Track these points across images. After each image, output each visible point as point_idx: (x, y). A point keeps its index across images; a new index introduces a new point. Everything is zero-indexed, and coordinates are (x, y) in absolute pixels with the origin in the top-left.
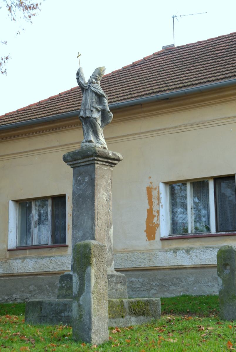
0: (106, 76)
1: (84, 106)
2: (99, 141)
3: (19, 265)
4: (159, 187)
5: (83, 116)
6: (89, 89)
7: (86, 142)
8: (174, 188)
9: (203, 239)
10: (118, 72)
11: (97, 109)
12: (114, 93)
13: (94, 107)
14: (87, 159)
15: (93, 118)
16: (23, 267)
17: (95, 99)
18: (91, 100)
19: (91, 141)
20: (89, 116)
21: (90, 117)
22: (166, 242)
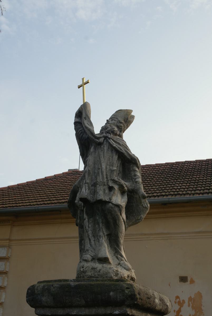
0: (21, 185)
1: (90, 177)
2: (122, 260)
5: (89, 198)
6: (105, 143)
7: (93, 259)
10: (32, 182)
11: (121, 187)
12: (32, 198)
13: (115, 182)
15: (113, 204)
17: (117, 166)
18: (108, 167)
19: (105, 260)
20: (104, 199)
21: (106, 203)
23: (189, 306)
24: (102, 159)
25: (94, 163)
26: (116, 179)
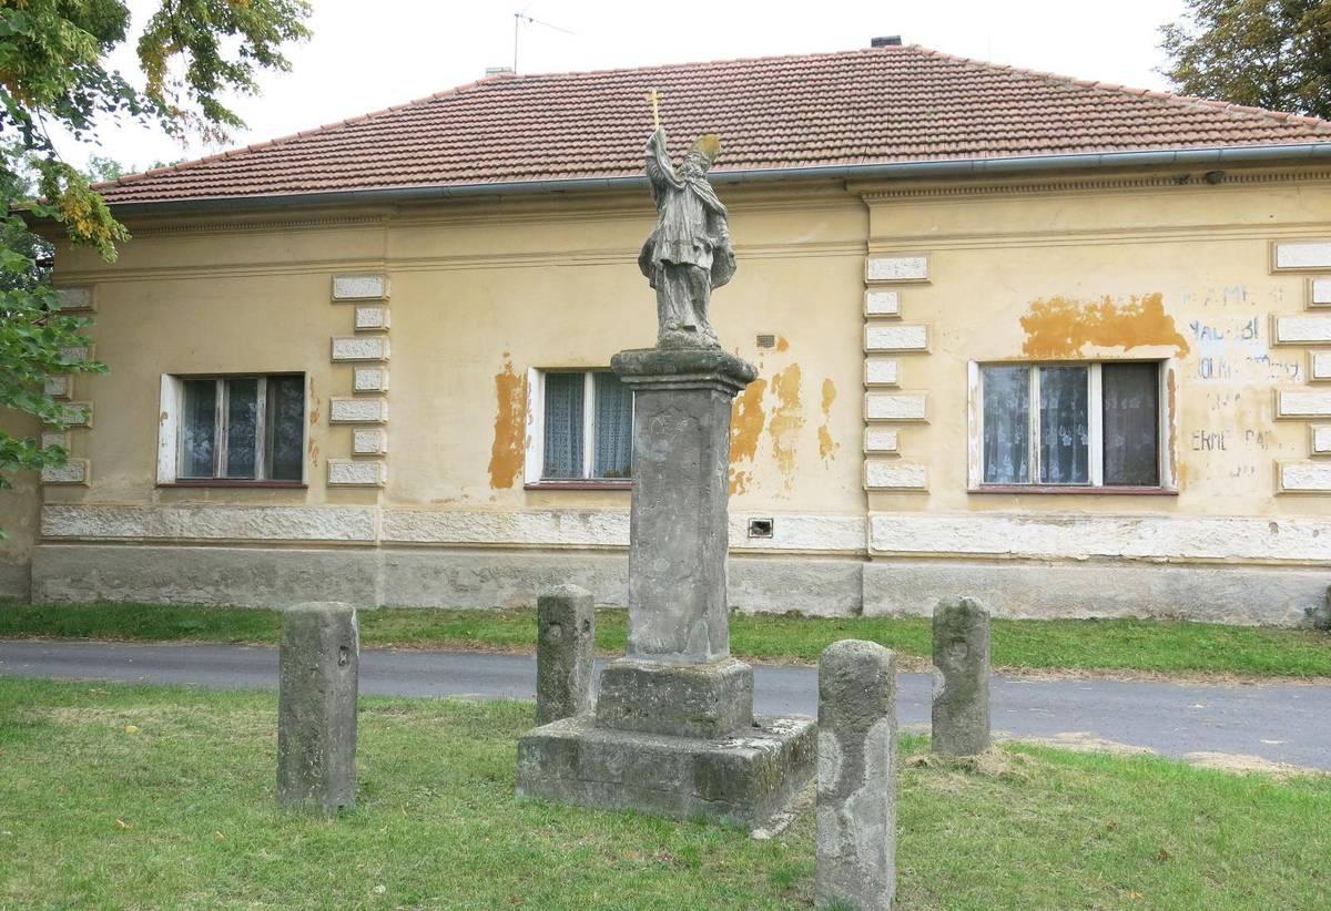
3: (186, 520)
4: (526, 377)
8: (562, 383)
9: (617, 494)
14: (693, 377)
16: (195, 525)
19: (692, 329)
22: (536, 495)
23: (773, 391)
24: (685, 211)
25: (675, 216)
26: (701, 236)
